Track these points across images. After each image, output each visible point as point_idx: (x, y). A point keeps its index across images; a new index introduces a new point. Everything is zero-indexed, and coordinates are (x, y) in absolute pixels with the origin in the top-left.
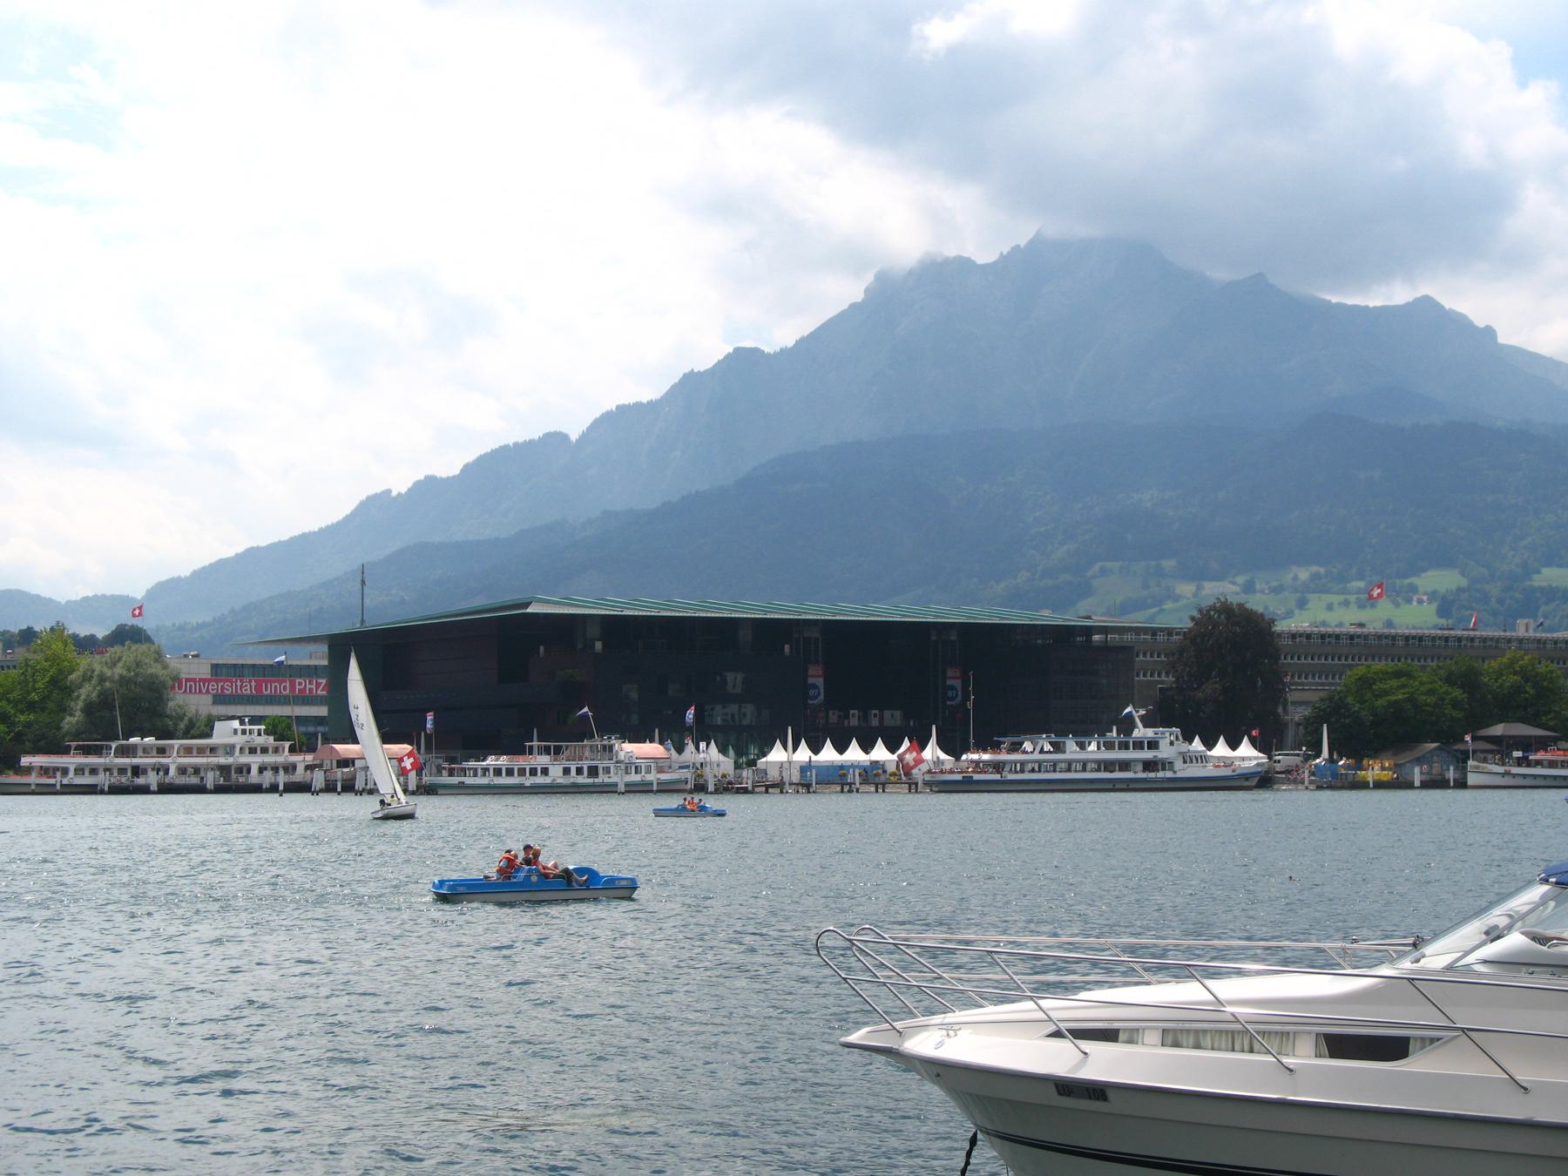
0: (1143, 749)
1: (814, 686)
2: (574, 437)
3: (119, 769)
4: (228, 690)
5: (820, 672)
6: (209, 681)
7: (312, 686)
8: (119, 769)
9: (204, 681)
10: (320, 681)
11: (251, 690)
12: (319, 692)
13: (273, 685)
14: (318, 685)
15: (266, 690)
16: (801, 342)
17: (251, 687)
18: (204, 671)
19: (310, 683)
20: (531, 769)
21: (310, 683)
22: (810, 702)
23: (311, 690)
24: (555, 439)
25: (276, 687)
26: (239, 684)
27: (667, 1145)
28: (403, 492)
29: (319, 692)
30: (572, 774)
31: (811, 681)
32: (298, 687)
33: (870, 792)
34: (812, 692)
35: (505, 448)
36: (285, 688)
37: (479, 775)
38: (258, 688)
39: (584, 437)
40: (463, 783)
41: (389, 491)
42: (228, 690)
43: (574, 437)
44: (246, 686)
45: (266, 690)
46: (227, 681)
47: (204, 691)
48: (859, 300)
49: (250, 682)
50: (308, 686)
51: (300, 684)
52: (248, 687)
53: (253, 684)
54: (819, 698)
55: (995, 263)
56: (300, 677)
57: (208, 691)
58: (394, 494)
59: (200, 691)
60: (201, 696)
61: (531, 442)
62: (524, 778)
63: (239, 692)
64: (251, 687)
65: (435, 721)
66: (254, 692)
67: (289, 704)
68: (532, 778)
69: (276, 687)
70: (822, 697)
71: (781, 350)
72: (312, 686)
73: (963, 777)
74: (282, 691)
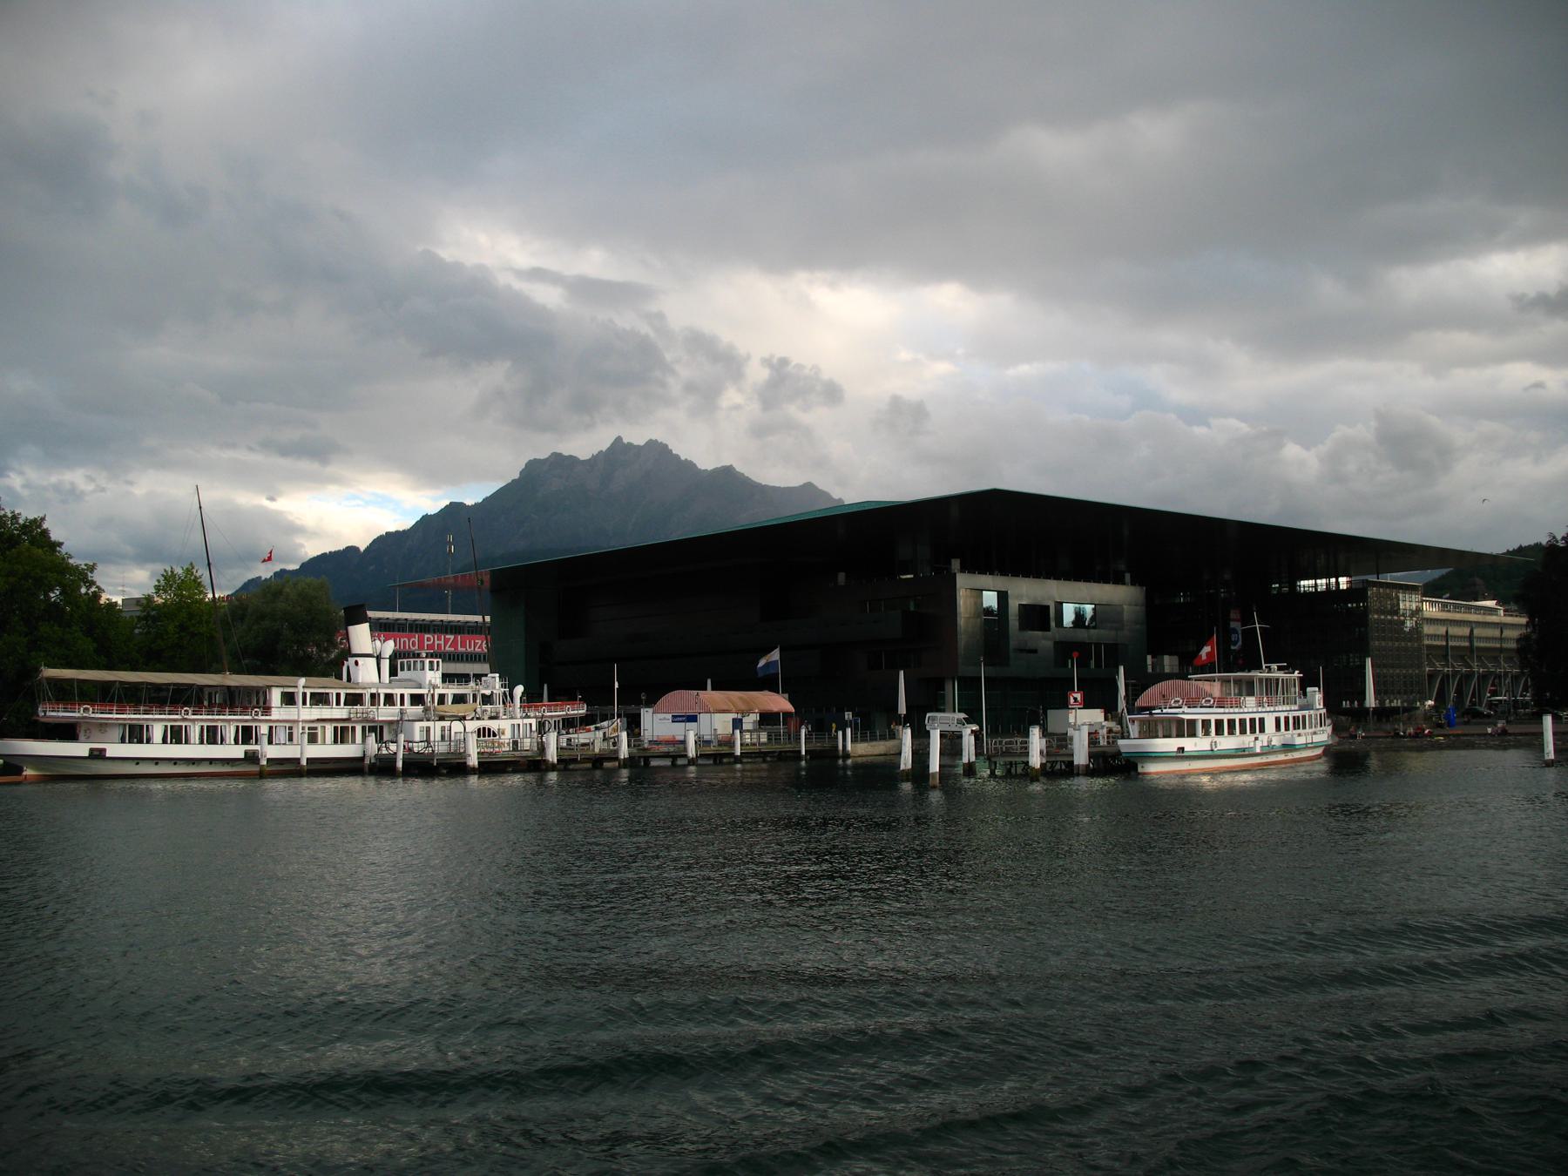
0: (181, 743)
1: (1235, 631)
2: (362, 549)
10: (447, 637)
12: (447, 648)
14: (446, 641)
16: (486, 500)
19: (439, 639)
21: (439, 639)
22: (1233, 648)
23: (439, 645)
24: (352, 550)
25: (404, 642)
28: (604, 450)
29: (447, 648)
32: (426, 643)
33: (1080, 736)
34: (1234, 637)
35: (325, 554)
37: (1200, 721)
39: (366, 550)
41: (260, 577)
43: (362, 549)
48: (582, 458)
50: (437, 642)
51: (429, 639)
55: (590, 459)
56: (429, 632)
58: (263, 579)
61: (339, 551)
65: (1275, 584)
67: (462, 661)
69: (404, 642)
70: (1240, 643)
71: (386, 533)
73: (246, 752)
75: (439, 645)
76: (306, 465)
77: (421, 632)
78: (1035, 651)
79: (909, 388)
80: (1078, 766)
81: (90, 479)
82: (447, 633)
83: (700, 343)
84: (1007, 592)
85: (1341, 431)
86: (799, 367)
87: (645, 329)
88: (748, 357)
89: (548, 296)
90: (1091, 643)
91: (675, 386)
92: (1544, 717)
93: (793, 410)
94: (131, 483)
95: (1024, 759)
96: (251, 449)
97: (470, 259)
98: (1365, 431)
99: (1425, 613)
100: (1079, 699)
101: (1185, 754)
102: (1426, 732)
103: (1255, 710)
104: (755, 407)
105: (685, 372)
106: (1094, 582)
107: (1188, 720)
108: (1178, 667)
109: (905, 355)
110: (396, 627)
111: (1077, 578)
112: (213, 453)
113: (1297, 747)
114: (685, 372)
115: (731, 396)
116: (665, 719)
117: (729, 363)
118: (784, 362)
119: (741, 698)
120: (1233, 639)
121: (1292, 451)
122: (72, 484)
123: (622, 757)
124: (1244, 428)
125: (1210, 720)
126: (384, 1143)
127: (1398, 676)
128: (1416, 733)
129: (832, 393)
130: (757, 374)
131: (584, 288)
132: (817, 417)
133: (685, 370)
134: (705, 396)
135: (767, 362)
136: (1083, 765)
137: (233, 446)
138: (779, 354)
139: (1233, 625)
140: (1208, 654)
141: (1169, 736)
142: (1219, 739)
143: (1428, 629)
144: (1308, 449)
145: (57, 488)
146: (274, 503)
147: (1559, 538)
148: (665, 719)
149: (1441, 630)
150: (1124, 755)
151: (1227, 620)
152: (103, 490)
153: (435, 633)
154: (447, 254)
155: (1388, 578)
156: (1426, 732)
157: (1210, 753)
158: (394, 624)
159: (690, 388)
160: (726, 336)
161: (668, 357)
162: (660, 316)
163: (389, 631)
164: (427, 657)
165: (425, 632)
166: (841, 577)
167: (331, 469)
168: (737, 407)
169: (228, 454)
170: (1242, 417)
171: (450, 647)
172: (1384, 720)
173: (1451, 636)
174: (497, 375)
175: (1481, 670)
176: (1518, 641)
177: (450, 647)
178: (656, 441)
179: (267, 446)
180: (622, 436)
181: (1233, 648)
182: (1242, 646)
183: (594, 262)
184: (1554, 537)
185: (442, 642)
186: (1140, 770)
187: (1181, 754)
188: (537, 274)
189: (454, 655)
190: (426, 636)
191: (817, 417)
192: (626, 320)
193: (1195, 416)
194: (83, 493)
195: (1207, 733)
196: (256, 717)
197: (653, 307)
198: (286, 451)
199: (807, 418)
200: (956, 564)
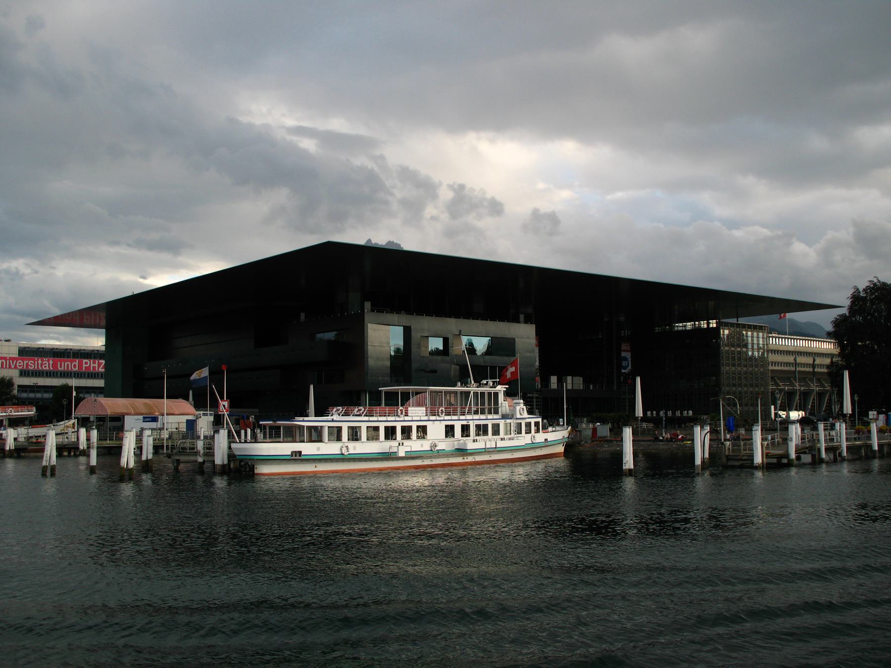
0: (307, 426)
1: (625, 359)
3: (328, 427)
4: (31, 366)
5: (629, 348)
6: (16, 359)
7: (94, 365)
8: (328, 427)
9: (13, 359)
10: (101, 361)
11: (49, 367)
13: (66, 364)
14: (99, 364)
15: (61, 367)
17: (49, 364)
18: (14, 353)
19: (94, 363)
20: (386, 428)
22: (623, 371)
23: (94, 368)
25: (68, 365)
26: (40, 362)
27: (168, 517)
30: (362, 440)
31: (623, 354)
32: (84, 366)
34: (624, 363)
36: (75, 366)
38: (54, 365)
40: (300, 452)
42: (31, 366)
44: (45, 364)
45: (61, 367)
46: (31, 360)
47: (13, 367)
49: (48, 361)
50: (92, 365)
51: (86, 363)
52: (47, 365)
53: (51, 362)
54: (628, 368)
56: (87, 358)
57: (16, 367)
59: (10, 367)
60: (10, 370)
62: (394, 444)
63: (40, 368)
64: (49, 364)
66: (51, 368)
67: (43, 376)
68: (406, 442)
69: (68, 365)
70: (630, 367)
72: (94, 365)
74: (73, 368)
75: (94, 368)
76: (166, 256)
77: (81, 358)
78: (435, 372)
79: (545, 206)
80: (217, 465)
81: (27, 265)
82: (101, 359)
83: (407, 175)
84: (411, 327)
85: (830, 235)
86: (472, 189)
87: (370, 165)
88: (440, 184)
89: (308, 145)
90: (487, 366)
91: (395, 206)
92: (695, 428)
93: (471, 219)
94: (54, 268)
95: (211, 459)
96: (129, 245)
97: (258, 121)
98: (846, 234)
99: (770, 346)
100: (226, 406)
101: (303, 457)
102: (680, 437)
103: (426, 418)
104: (445, 217)
105: (399, 194)
106: (445, 317)
107: (308, 427)
108: (556, 385)
109: (541, 186)
110: (93, 356)
111: (493, 319)
112: (106, 249)
113: (469, 451)
114: (399, 194)
115: (430, 210)
116: (139, 419)
117: (428, 188)
118: (462, 187)
119: (145, 404)
120: (624, 365)
121: (798, 247)
122: (17, 269)
123: (8, 448)
124: (766, 232)
125: (488, 425)
126: (769, 579)
127: (746, 393)
128: (671, 438)
129: (496, 208)
130: (446, 195)
131: (330, 139)
132: (486, 223)
133: (400, 192)
134: (413, 209)
135: (451, 187)
136: (219, 465)
137: (116, 243)
138: (460, 181)
139: (623, 354)
140: (512, 373)
141: (303, 442)
142: (537, 435)
143: (772, 358)
144: (810, 247)
145: (7, 272)
146: (146, 280)
147: (861, 290)
148: (139, 419)
149: (790, 359)
150: (238, 457)
151: (619, 351)
152: (36, 272)
153: (91, 358)
154: (244, 119)
155: (742, 321)
156: (680, 437)
157: (341, 456)
158: (91, 354)
159: (404, 203)
160: (424, 171)
161: (388, 183)
162: (382, 157)
163: (58, 357)
164: (741, 381)
165: (84, 358)
166: (303, 316)
167: (181, 259)
168: (433, 218)
169: (113, 250)
170: (764, 226)
171: (102, 369)
172: (677, 426)
173: (799, 364)
174: (281, 196)
175: (802, 388)
176: (828, 367)
177: (102, 369)
178: (393, 242)
179: (139, 244)
180: (371, 239)
181: (623, 371)
182: (631, 369)
183: (338, 124)
184: (858, 289)
185: (96, 365)
186: (256, 471)
187: (296, 456)
188: (300, 131)
189: (78, 374)
190: (85, 361)
191: (486, 223)
192: (360, 161)
193: (732, 224)
194: (23, 274)
195: (528, 431)
196: (11, 414)
197: (377, 153)
198: (153, 246)
199: (480, 224)
200: (368, 305)
